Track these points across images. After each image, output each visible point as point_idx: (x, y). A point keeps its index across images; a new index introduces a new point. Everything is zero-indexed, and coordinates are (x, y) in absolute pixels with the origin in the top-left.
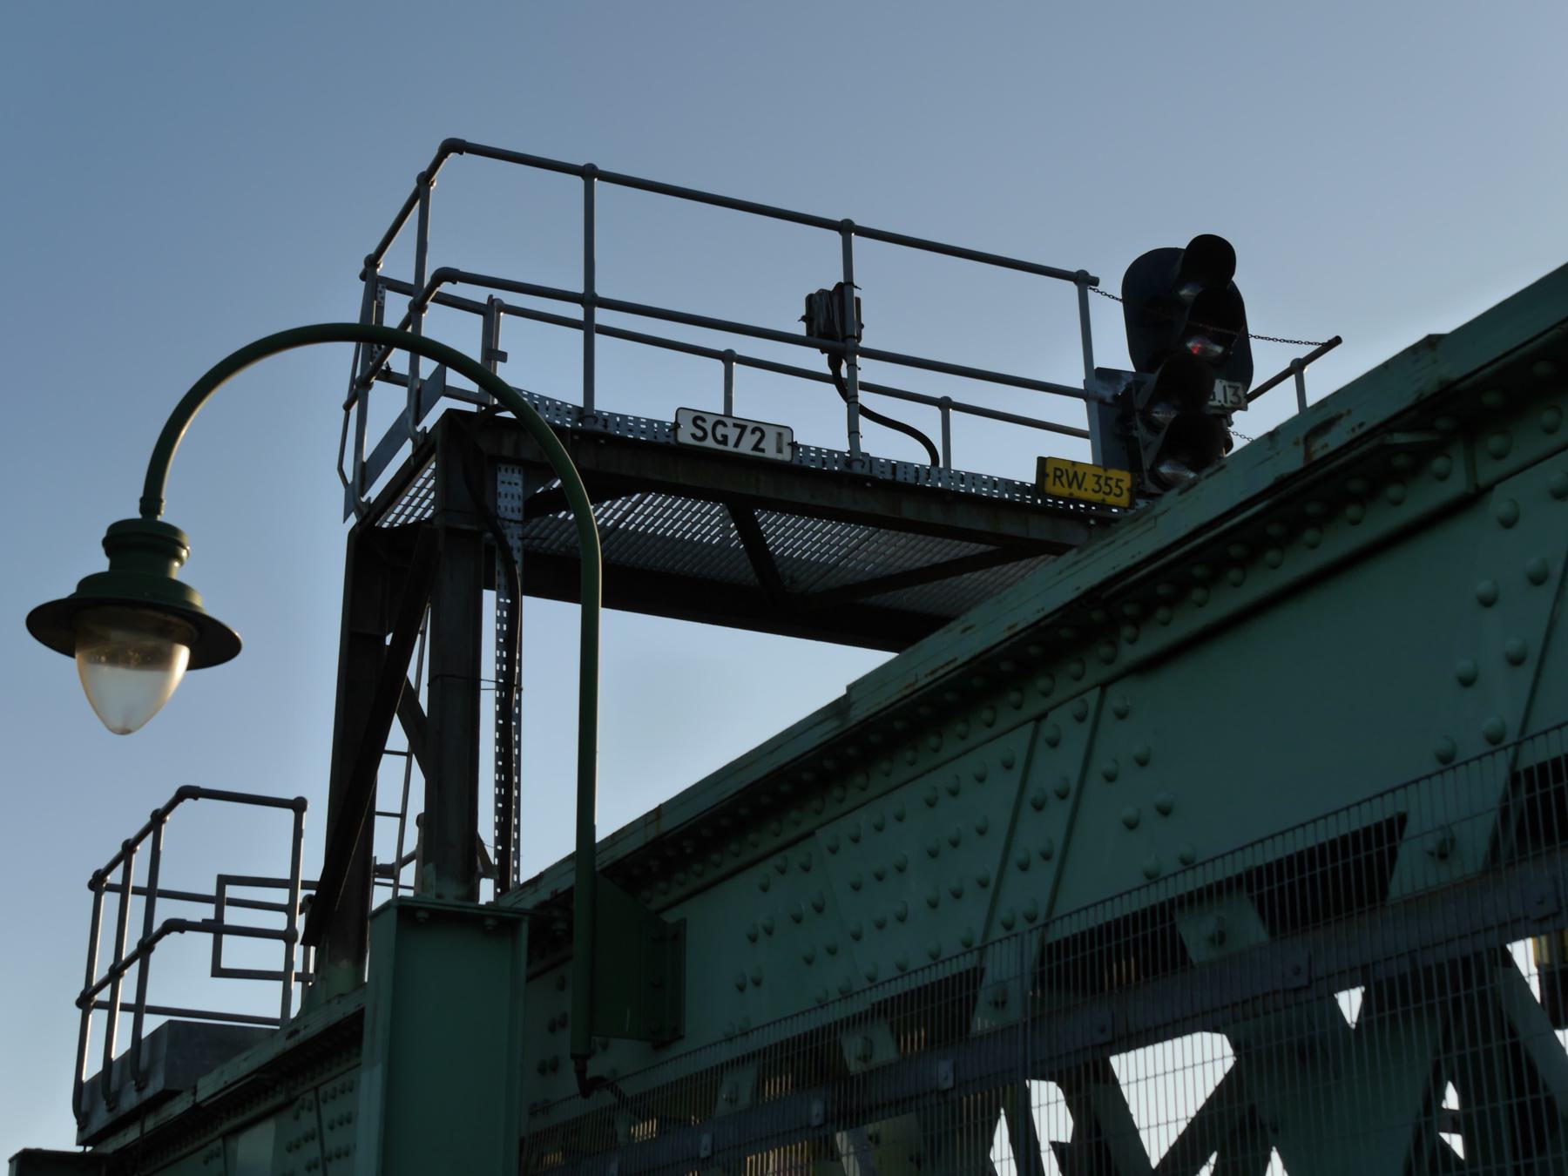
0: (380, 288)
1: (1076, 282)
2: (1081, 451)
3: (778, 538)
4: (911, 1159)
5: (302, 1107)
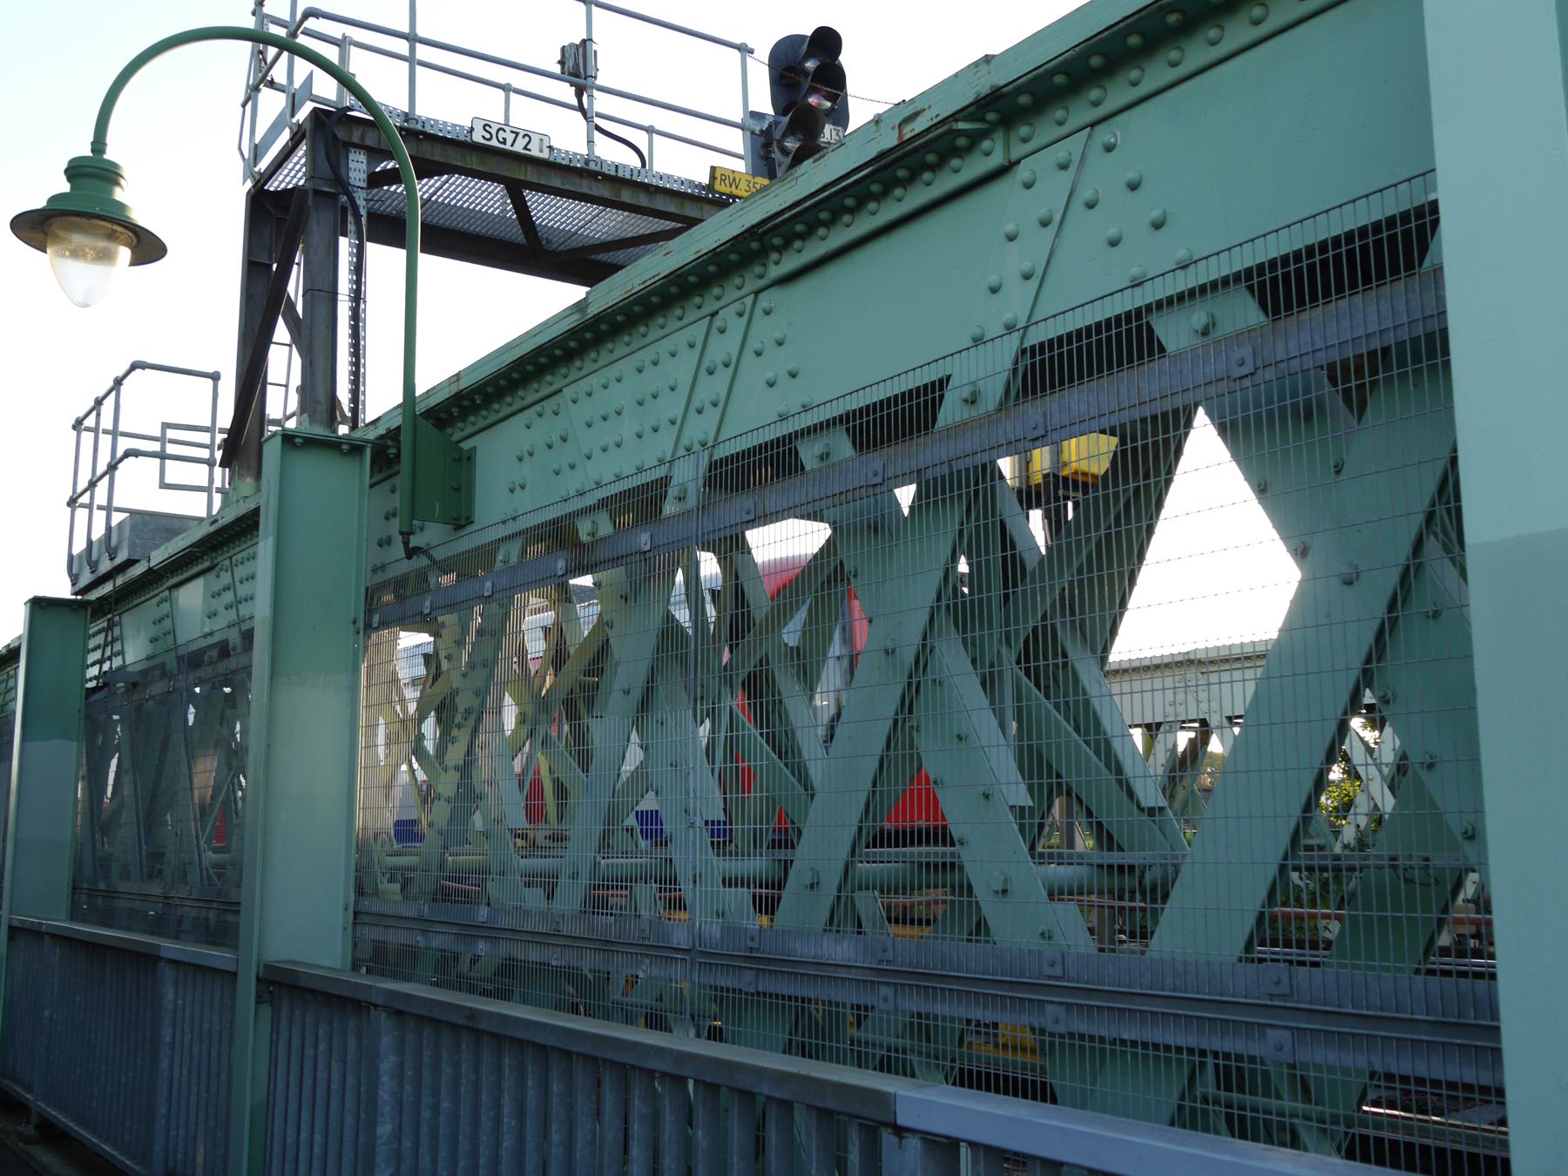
0: (265, 22)
1: (739, 50)
2: (740, 166)
3: (539, 211)
4: (622, 597)
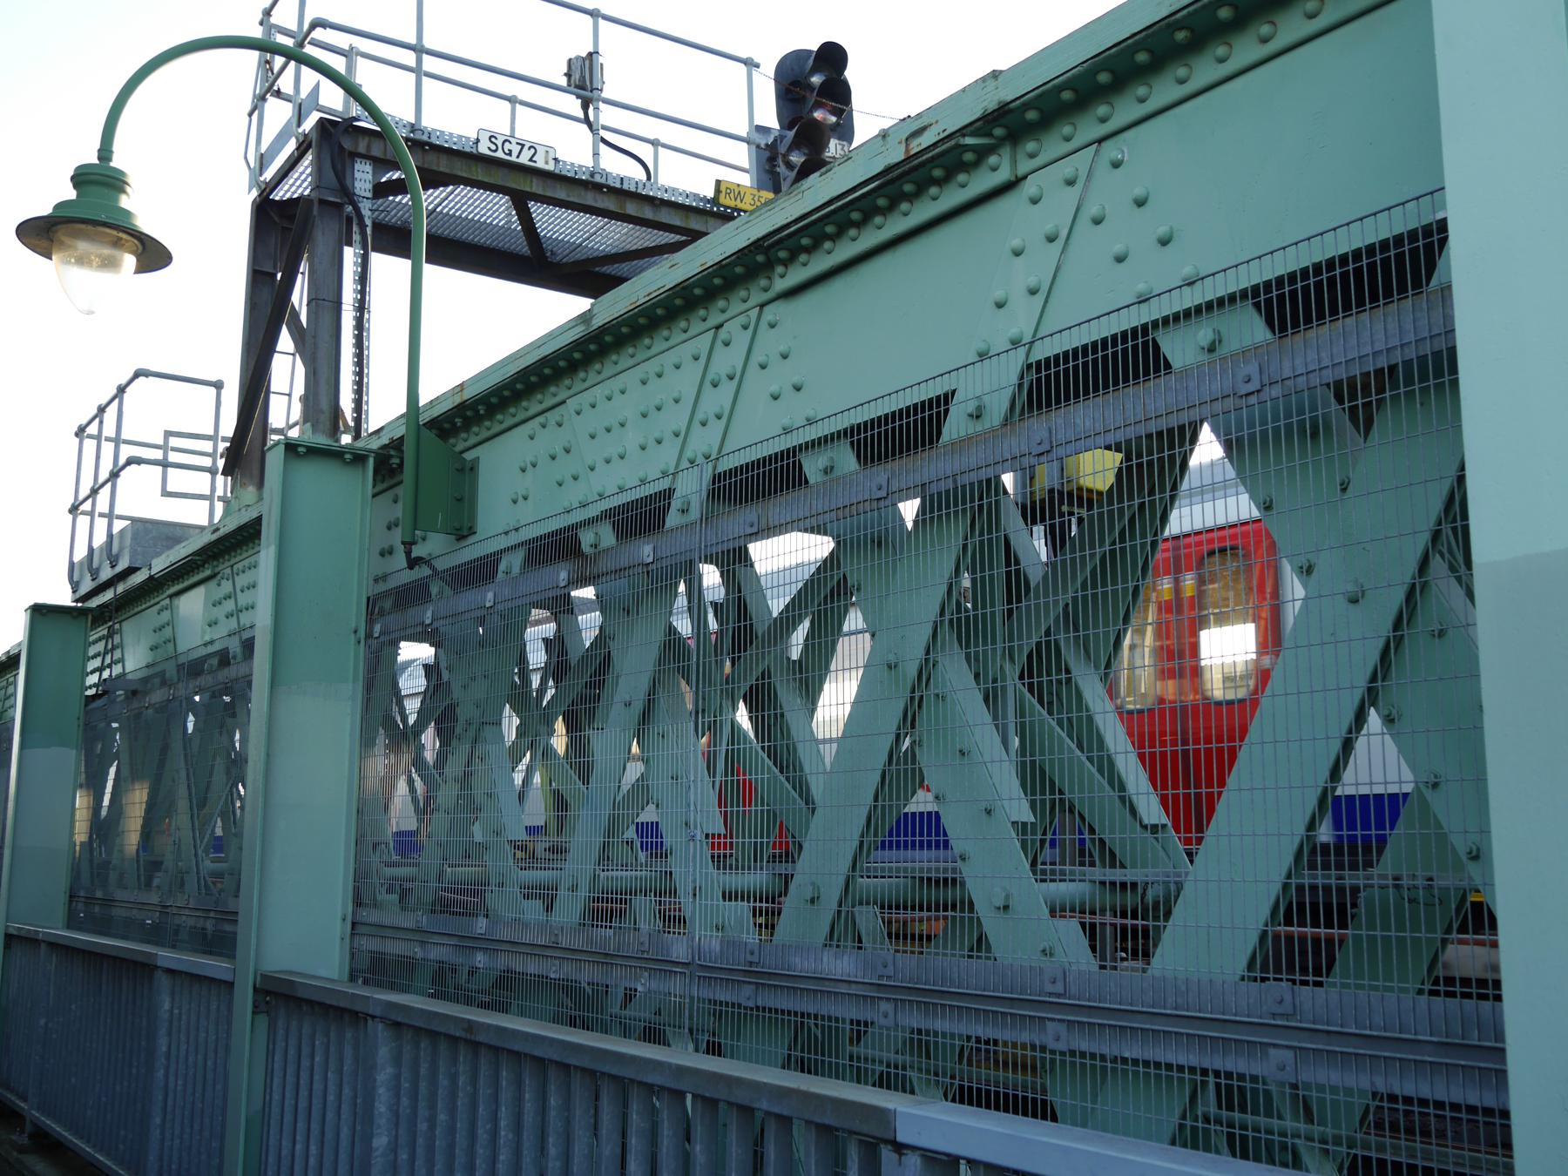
2: (745, 180)
3: (544, 223)
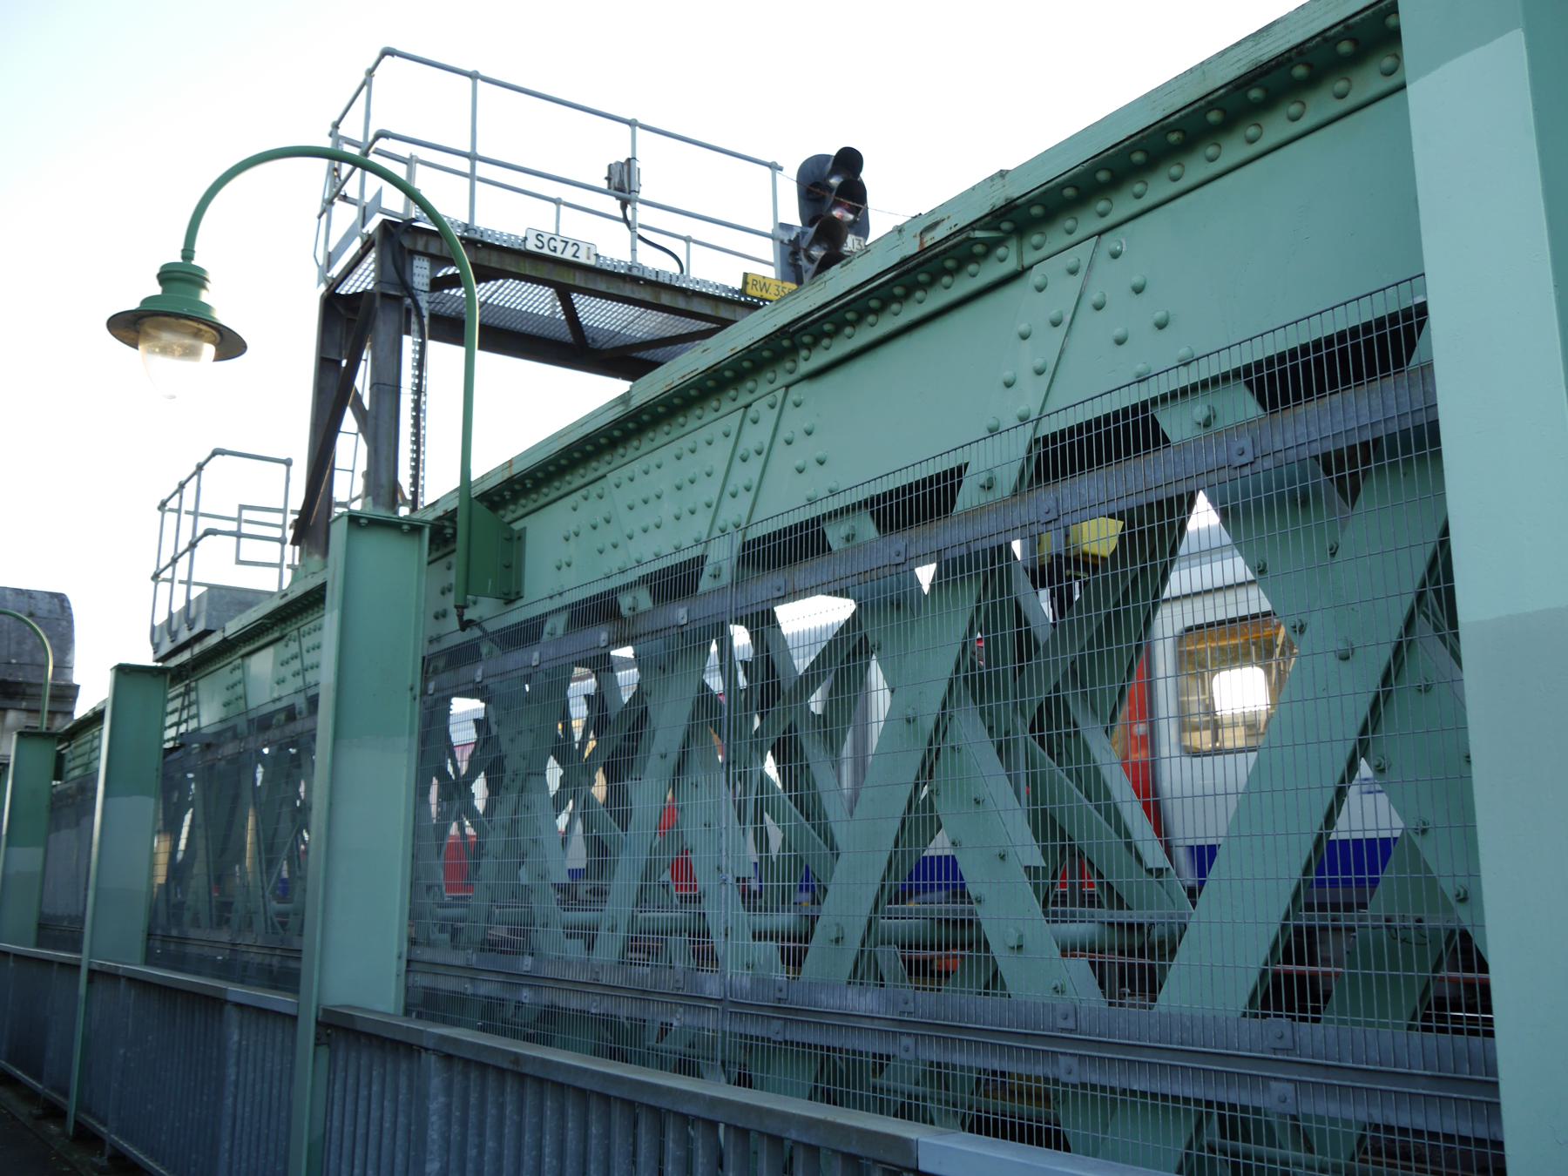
5: (290, 640)
